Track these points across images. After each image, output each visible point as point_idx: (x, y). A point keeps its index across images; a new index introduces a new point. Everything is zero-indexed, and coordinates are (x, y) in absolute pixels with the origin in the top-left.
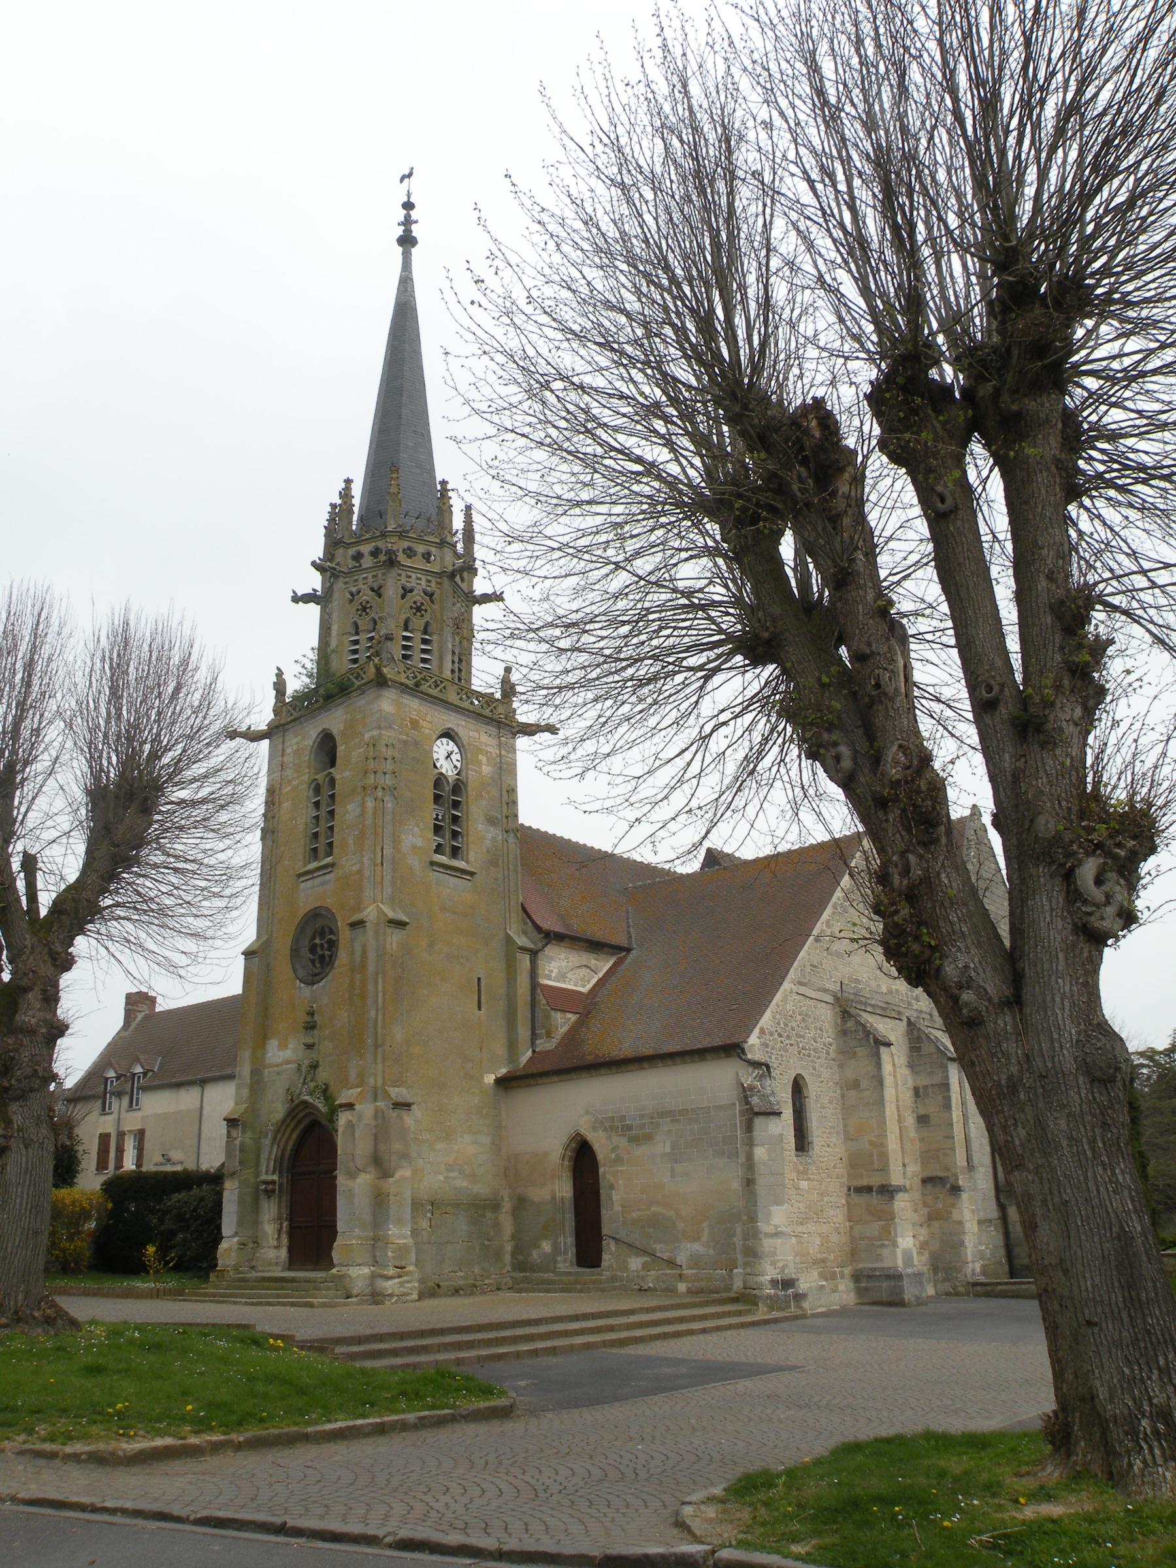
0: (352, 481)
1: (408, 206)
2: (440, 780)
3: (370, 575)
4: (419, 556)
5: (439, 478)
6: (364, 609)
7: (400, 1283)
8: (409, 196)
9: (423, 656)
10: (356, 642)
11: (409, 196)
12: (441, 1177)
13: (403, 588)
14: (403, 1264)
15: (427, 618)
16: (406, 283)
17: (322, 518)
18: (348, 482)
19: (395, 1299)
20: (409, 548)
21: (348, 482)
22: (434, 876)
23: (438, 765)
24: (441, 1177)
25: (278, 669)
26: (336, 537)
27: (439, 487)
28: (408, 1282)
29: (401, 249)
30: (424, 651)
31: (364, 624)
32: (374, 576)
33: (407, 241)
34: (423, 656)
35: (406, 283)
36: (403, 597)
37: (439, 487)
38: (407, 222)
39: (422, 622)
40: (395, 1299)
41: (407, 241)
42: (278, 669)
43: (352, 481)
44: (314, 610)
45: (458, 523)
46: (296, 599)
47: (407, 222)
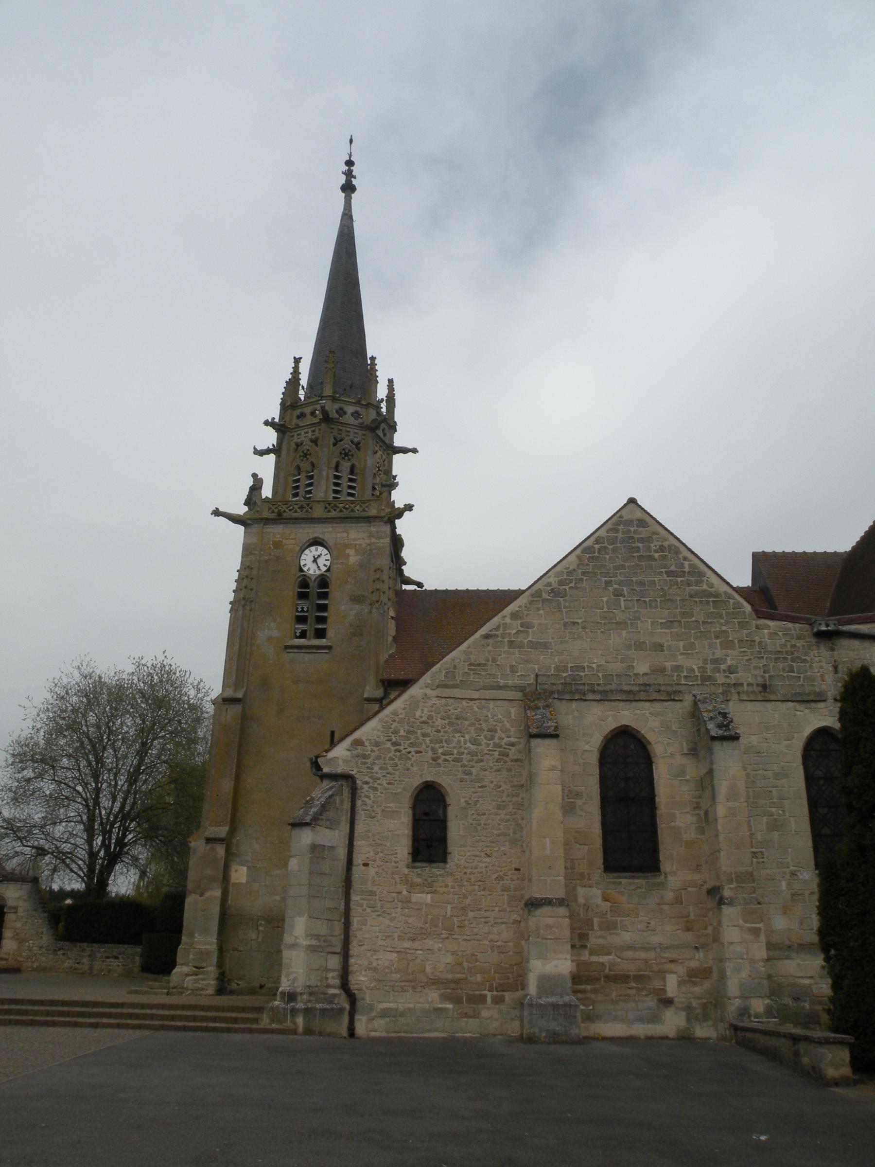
0: (375, 358)
1: (350, 163)
2: (304, 582)
3: (310, 430)
4: (308, 416)
5: (369, 356)
6: (305, 455)
7: (195, 980)
8: (350, 156)
9: (350, 491)
10: (298, 481)
11: (350, 156)
12: (277, 898)
13: (335, 438)
14: (203, 965)
15: (354, 461)
16: (347, 216)
17: (281, 388)
18: (297, 361)
19: (190, 992)
20: (357, 412)
21: (297, 361)
22: (287, 657)
23: (305, 569)
24: (277, 898)
25: (255, 476)
26: (290, 402)
27: (369, 362)
28: (203, 980)
29: (344, 195)
30: (350, 487)
31: (305, 466)
32: (313, 431)
33: (348, 188)
34: (350, 491)
35: (347, 216)
36: (334, 445)
37: (369, 362)
38: (349, 174)
39: (349, 464)
40: (190, 992)
41: (348, 188)
42: (255, 476)
43: (375, 358)
44: (272, 457)
45: (382, 392)
46: (415, 451)
47: (349, 174)
